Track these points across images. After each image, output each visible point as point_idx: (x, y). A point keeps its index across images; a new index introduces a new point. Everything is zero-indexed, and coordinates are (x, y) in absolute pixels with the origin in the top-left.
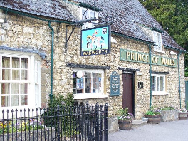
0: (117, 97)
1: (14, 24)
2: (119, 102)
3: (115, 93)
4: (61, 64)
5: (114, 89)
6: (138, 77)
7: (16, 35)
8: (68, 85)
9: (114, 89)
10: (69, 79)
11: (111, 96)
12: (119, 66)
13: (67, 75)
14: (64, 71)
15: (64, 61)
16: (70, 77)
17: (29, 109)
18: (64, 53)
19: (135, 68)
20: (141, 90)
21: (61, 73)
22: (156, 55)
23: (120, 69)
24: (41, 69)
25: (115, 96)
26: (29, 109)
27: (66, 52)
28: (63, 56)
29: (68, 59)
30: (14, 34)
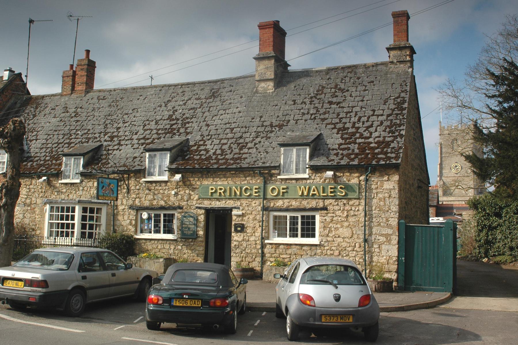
0: (194, 240)
1: (88, 182)
2: (198, 246)
3: (187, 235)
4: (123, 207)
5: (186, 231)
6: (234, 218)
7: (89, 189)
8: (131, 225)
9: (186, 231)
10: (131, 220)
11: (183, 238)
12: (197, 205)
13: (129, 217)
14: (127, 213)
15: (126, 205)
16: (132, 219)
17: (253, 58)
18: (126, 198)
19: (230, 206)
20: (241, 234)
21: (123, 215)
22: (421, 169)
23: (200, 208)
24: (107, 212)
25: (190, 239)
26: (253, 58)
27: (128, 197)
28: (125, 201)
29: (130, 202)
30: (328, 249)
